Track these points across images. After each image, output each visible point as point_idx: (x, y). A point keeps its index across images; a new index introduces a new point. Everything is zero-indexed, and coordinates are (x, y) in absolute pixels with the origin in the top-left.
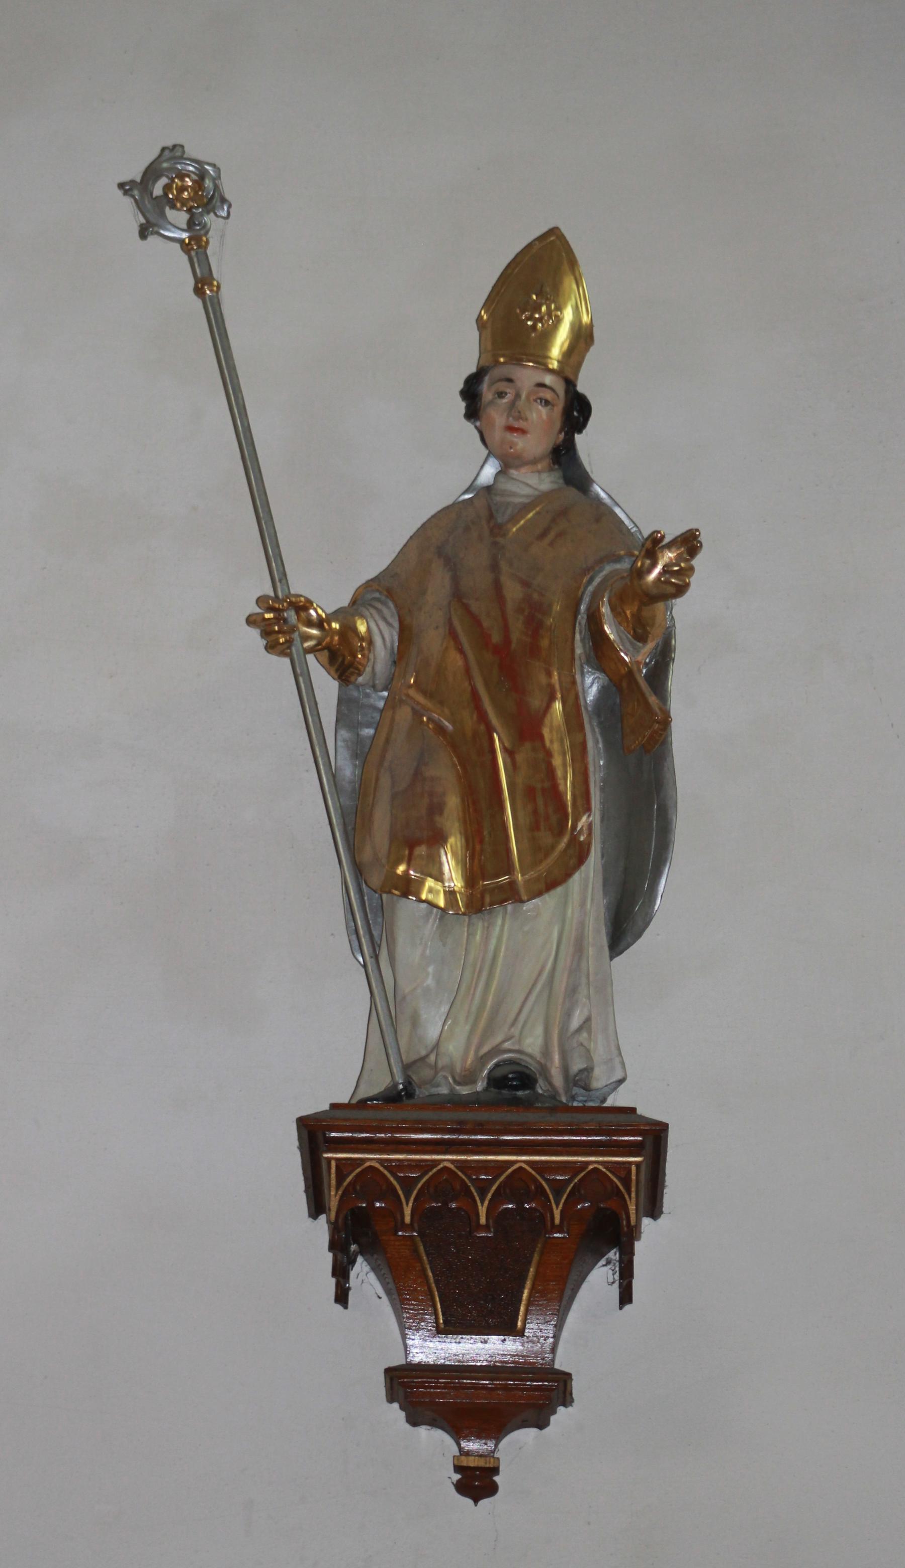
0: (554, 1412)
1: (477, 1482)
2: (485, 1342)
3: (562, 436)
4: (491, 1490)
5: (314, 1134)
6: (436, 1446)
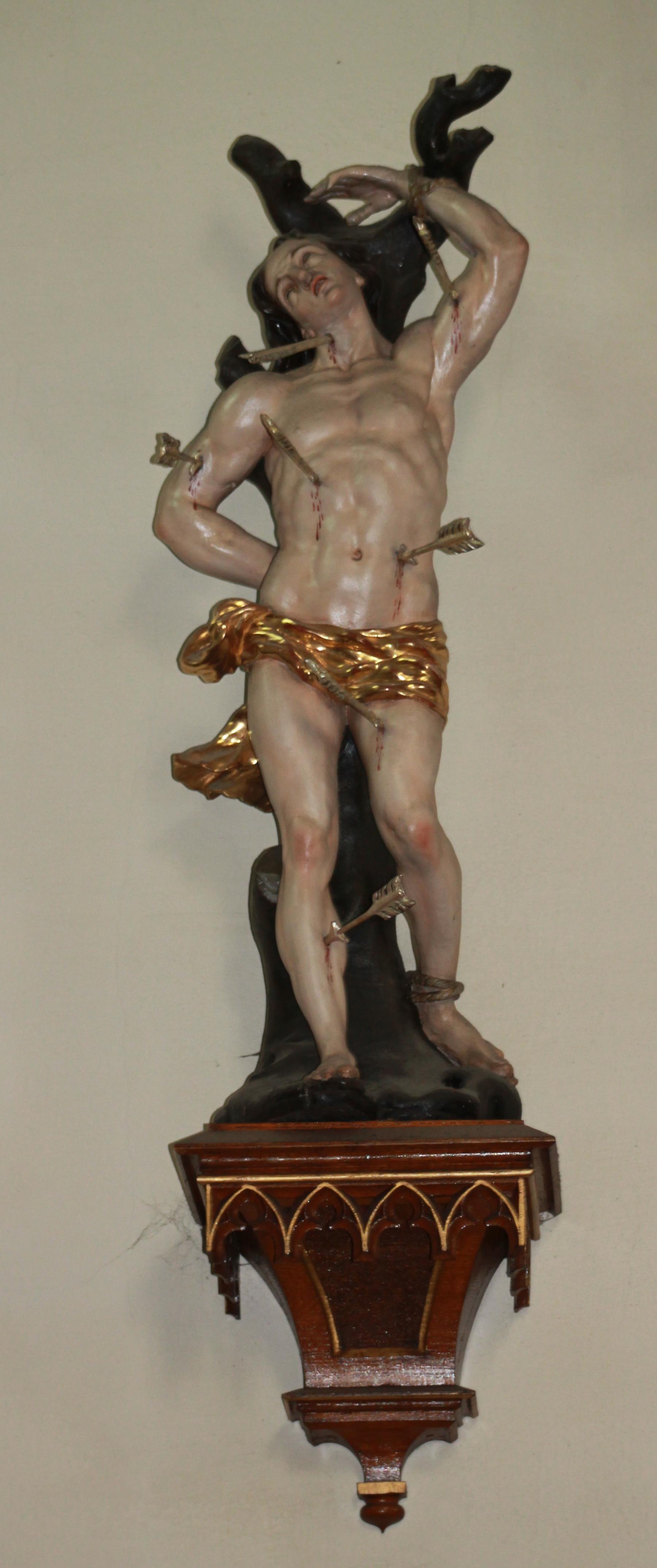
0: (460, 1424)
1: (382, 1511)
2: (386, 892)
3: (345, 634)
4: (398, 1515)
5: (190, 1157)
6: (339, 1471)
